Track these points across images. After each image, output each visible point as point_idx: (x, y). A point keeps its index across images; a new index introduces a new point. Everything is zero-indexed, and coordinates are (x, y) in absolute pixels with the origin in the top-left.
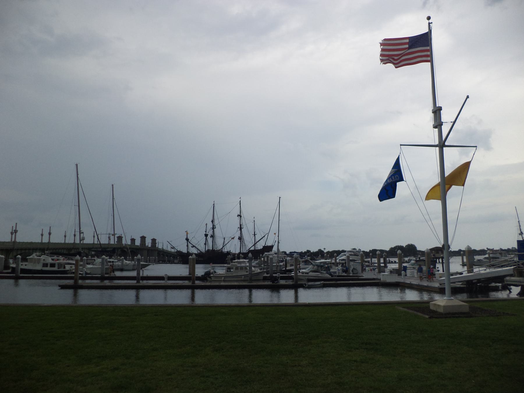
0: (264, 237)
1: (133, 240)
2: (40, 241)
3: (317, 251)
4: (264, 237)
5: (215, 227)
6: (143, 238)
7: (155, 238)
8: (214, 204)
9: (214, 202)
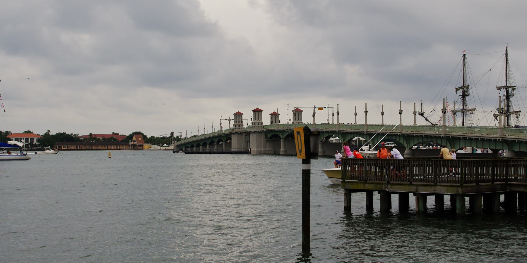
1: (275, 116)
3: (69, 135)
5: (467, 94)
6: (257, 112)
8: (464, 55)
9: (465, 51)
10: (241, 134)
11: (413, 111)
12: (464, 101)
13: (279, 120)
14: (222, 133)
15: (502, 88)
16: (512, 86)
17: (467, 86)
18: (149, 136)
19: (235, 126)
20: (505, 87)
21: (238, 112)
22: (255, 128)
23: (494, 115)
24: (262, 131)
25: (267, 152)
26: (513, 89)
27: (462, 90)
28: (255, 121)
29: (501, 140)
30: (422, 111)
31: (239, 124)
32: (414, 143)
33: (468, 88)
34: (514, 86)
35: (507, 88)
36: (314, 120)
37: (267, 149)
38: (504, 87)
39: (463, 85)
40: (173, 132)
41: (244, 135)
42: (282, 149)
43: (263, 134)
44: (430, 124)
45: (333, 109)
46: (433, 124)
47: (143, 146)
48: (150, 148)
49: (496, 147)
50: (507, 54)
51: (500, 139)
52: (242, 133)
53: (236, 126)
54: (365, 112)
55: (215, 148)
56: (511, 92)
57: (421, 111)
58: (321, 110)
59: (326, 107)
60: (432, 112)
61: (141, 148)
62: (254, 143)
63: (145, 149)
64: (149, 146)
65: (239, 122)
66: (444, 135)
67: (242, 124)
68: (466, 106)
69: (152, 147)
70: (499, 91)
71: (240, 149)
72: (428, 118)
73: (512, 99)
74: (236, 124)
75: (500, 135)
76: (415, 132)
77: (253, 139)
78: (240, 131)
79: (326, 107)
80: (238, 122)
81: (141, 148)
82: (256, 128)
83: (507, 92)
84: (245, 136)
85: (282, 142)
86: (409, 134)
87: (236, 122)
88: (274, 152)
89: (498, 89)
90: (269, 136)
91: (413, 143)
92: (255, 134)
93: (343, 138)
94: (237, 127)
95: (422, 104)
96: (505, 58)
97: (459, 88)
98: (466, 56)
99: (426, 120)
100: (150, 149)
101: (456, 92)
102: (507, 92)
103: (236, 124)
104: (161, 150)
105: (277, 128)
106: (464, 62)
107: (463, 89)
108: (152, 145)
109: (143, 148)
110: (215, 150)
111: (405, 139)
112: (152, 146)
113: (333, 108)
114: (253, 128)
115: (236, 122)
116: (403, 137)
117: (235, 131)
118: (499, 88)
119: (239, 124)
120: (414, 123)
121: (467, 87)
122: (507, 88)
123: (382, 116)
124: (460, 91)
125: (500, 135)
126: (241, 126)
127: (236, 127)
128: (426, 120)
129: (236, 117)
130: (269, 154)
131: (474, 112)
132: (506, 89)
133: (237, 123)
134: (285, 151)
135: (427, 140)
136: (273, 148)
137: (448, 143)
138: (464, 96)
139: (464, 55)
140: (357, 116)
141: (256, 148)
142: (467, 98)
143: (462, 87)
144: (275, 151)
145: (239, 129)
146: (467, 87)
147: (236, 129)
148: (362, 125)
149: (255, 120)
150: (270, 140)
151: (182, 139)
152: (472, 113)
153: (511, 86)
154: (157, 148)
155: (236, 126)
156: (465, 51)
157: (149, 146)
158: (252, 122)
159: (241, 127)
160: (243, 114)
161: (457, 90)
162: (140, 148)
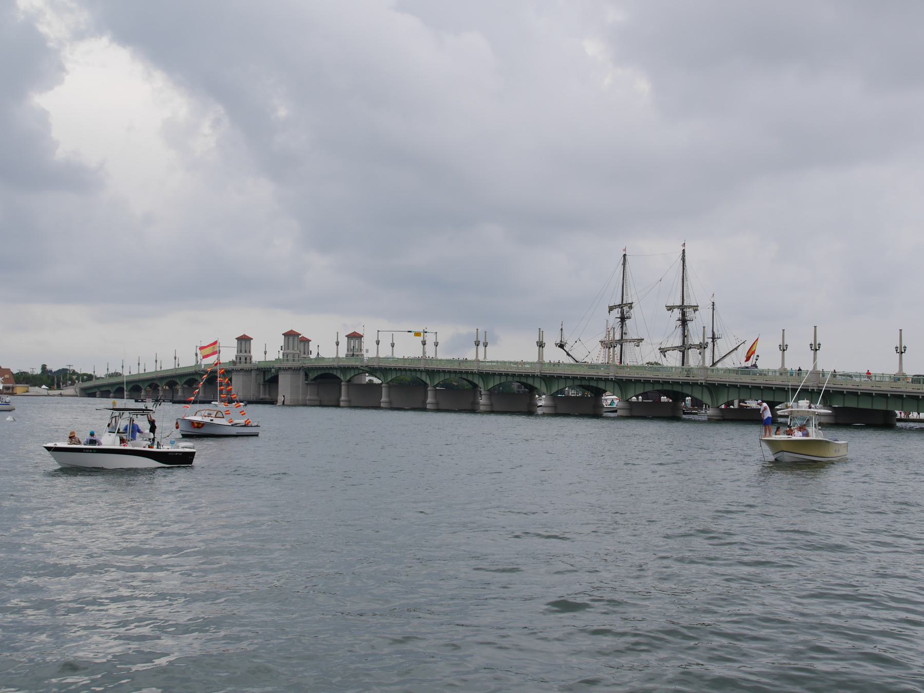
0: (736, 349)
2: (420, 355)
4: (736, 349)
7: (293, 330)
8: (625, 255)
9: (625, 250)
10: (249, 371)
11: (336, 341)
12: (622, 327)
13: (310, 349)
14: (200, 369)
15: (674, 308)
16: (693, 306)
17: (630, 304)
18: (15, 371)
19: (238, 359)
20: (680, 306)
21: (245, 335)
22: (287, 362)
23: (660, 349)
24: (300, 368)
25: (308, 402)
26: (695, 310)
27: (620, 310)
28: (288, 351)
29: (817, 390)
30: (563, 340)
31: (246, 354)
32: (558, 387)
33: (631, 307)
34: (696, 305)
35: (682, 308)
36: (541, 355)
37: (308, 397)
38: (678, 307)
39: (622, 302)
40: (45, 364)
41: (253, 373)
42: (383, 399)
43: (301, 371)
44: (572, 362)
45: (436, 335)
46: (576, 361)
47: (13, 388)
48: (27, 392)
49: (774, 399)
50: (685, 256)
51: (539, 374)
52: (251, 370)
53: (240, 358)
54: (537, 342)
55: (180, 394)
56: (690, 313)
57: (561, 341)
58: (418, 336)
59: (411, 332)
60: (576, 342)
61: (10, 391)
62: (238, 385)
63: (17, 394)
64: (25, 389)
65: (246, 352)
66: (476, 371)
67: (249, 355)
68: (625, 334)
69: (30, 391)
70: (670, 312)
71: (248, 397)
72: (570, 353)
73: (690, 324)
74: (241, 354)
75: (816, 383)
76: (393, 365)
77: (284, 381)
78: (248, 366)
79: (411, 332)
80: (243, 351)
81: (10, 391)
82: (290, 363)
83: (684, 314)
84: (257, 374)
85: (383, 388)
86: (725, 383)
87: (241, 351)
88: (319, 402)
89: (669, 310)
90: (312, 376)
91: (557, 385)
92: (290, 372)
93: (430, 377)
94: (243, 360)
95: (562, 330)
96: (682, 262)
97: (615, 306)
98: (627, 257)
99: (568, 354)
100: (26, 394)
101: (609, 312)
102: (684, 314)
103: (241, 354)
104: (48, 395)
105: (336, 364)
106: (624, 267)
107: (622, 308)
108: (31, 386)
109: (15, 392)
110: (201, 397)
111: (429, 375)
112: (30, 388)
113: (436, 333)
114: (285, 363)
115: (241, 351)
116: (427, 373)
117: (239, 366)
118: (670, 308)
119: (246, 354)
120: (537, 359)
121: (629, 305)
122: (682, 308)
123: (391, 348)
124: (615, 311)
125: (816, 383)
126: (248, 358)
127: (240, 359)
128: (568, 354)
129: (241, 344)
130: (312, 406)
131: (641, 343)
132: (683, 310)
133: (243, 354)
134: (390, 402)
135: (507, 380)
136: (318, 395)
137: (428, 376)
138: (623, 319)
139: (625, 255)
140: (339, 346)
141: (289, 396)
142: (628, 322)
143: (619, 305)
144: (320, 401)
145: (246, 363)
146: (629, 305)
147: (240, 363)
148: (419, 359)
149: (288, 349)
150: (313, 382)
151: (97, 378)
152: (638, 346)
153: (691, 305)
154: (39, 393)
155: (240, 358)
156: (625, 250)
157: (25, 389)
158: (283, 353)
159: (248, 361)
160: (252, 339)
161: (611, 309)
162: (8, 392)
